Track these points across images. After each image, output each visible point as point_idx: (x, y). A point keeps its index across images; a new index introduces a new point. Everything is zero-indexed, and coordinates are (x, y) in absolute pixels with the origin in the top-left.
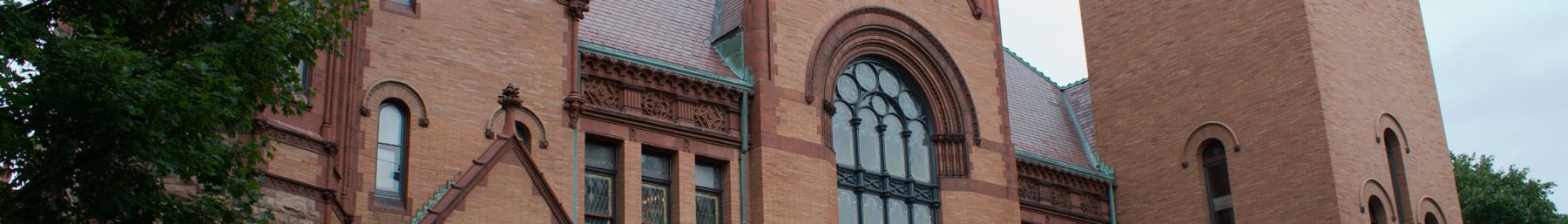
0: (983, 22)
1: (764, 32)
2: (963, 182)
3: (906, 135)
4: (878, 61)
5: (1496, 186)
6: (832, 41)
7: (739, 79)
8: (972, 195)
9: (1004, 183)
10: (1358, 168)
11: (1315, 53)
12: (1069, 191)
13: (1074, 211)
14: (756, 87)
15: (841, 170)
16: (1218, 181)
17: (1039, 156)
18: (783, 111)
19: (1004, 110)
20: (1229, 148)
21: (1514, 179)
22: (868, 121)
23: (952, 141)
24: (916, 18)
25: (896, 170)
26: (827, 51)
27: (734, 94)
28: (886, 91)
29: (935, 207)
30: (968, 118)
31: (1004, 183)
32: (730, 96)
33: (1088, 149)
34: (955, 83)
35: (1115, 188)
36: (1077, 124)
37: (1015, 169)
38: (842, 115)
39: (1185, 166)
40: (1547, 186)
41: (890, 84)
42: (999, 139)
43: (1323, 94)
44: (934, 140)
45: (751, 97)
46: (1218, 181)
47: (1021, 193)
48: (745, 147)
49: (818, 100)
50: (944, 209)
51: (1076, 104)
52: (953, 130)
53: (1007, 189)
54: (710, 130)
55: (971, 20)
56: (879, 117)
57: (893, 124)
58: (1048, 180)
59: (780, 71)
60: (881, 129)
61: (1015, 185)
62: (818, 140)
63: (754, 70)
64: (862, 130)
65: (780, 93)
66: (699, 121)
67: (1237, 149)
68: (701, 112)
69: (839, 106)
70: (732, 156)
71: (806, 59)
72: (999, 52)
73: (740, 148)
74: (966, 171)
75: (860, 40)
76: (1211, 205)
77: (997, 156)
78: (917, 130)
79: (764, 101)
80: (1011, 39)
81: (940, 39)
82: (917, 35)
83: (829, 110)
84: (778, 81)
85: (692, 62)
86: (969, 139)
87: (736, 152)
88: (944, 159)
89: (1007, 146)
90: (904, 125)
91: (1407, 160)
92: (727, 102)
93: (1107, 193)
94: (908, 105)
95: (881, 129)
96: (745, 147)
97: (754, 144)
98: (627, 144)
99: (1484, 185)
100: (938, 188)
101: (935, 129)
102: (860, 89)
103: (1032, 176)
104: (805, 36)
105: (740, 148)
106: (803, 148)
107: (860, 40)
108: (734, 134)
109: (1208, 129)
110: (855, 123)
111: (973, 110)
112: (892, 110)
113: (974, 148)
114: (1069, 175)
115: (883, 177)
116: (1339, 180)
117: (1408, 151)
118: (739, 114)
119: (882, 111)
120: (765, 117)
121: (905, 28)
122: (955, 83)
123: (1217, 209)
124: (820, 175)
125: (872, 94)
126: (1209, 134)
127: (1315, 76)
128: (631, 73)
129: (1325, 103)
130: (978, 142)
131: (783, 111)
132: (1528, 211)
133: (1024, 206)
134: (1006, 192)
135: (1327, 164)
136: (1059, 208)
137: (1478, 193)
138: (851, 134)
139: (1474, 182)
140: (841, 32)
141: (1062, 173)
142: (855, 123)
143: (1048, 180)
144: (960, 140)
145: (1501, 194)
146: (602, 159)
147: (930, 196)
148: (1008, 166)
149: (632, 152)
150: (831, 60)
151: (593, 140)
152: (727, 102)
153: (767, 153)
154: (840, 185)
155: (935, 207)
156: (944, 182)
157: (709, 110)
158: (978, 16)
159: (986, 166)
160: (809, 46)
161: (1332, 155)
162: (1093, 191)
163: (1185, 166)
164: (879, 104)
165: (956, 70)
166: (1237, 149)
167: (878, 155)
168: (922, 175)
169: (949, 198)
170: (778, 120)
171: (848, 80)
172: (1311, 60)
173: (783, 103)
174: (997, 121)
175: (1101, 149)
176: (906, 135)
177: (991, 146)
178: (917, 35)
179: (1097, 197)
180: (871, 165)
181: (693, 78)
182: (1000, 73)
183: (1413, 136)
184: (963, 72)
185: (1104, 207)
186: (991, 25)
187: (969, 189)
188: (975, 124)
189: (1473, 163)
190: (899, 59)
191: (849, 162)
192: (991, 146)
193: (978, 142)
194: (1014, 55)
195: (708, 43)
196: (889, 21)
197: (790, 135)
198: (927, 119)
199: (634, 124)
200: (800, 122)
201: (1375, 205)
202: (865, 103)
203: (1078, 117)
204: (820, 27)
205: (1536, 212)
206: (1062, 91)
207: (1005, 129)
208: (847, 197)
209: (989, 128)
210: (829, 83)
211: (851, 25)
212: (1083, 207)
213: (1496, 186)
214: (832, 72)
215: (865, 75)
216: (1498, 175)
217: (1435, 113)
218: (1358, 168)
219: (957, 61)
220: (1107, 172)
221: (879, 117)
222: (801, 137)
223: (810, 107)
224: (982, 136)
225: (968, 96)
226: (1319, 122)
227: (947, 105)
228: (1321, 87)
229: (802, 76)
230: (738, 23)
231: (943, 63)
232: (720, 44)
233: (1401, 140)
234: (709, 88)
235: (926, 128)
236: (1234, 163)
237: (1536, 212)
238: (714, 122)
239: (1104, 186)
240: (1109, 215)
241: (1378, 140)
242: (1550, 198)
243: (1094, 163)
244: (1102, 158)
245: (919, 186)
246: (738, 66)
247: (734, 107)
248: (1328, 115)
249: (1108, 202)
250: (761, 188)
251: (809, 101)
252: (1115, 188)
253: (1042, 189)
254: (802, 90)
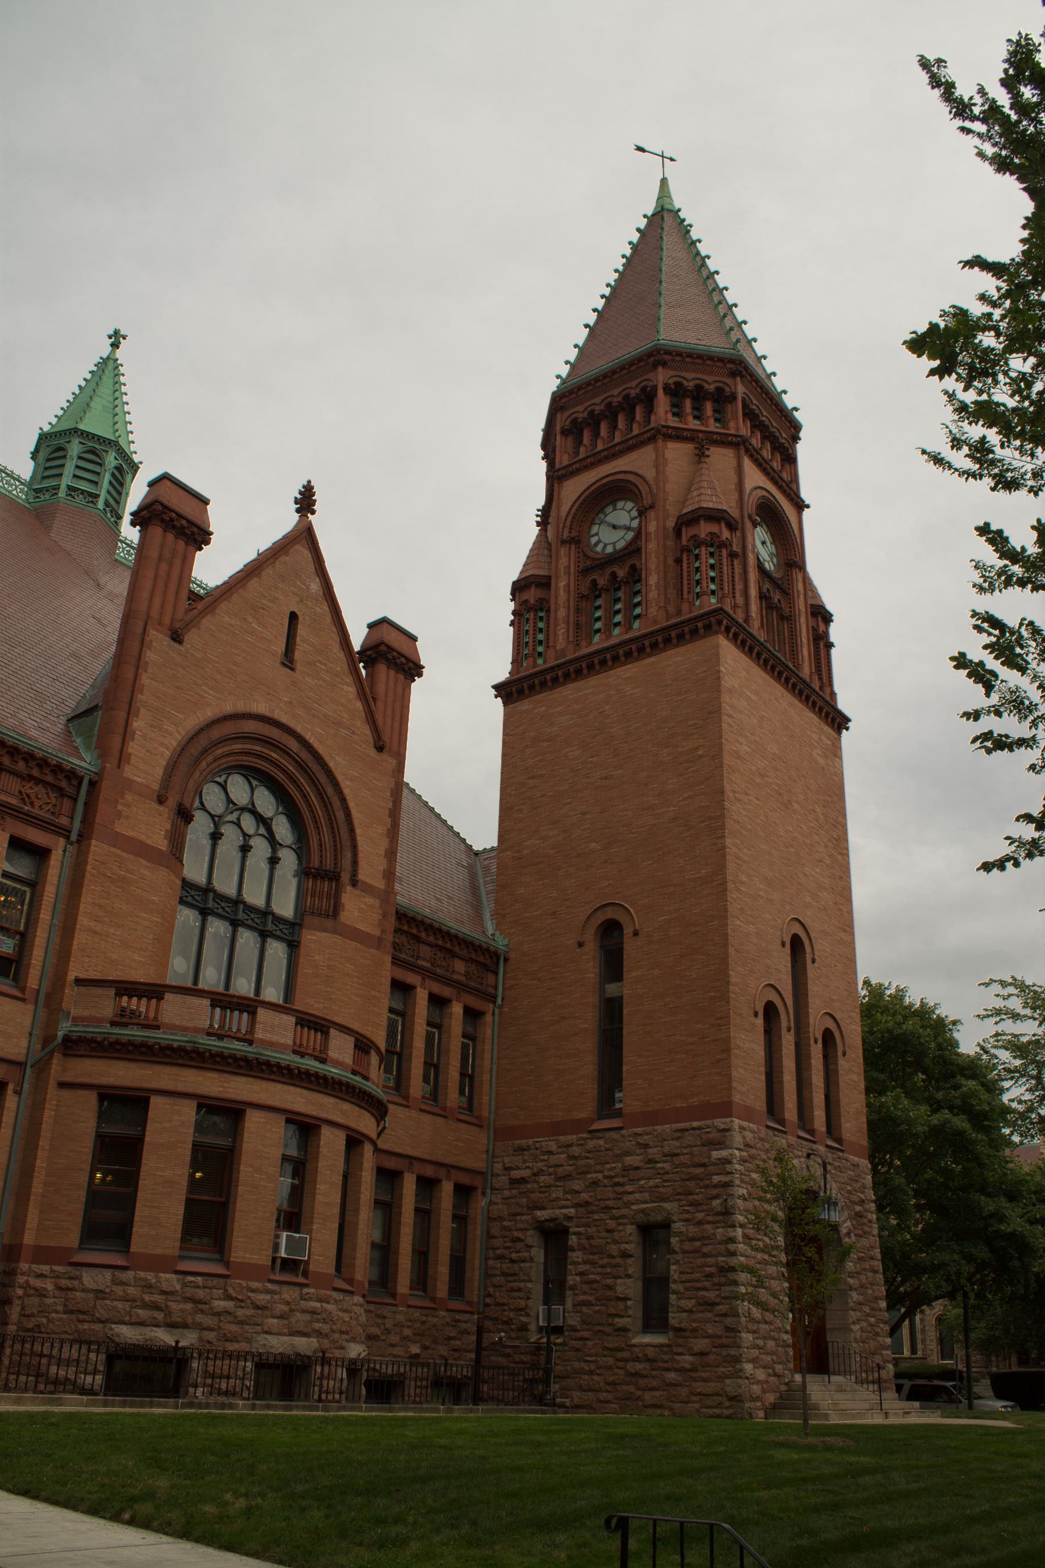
0: (384, 756)
1: (123, 715)
2: (329, 923)
3: (274, 861)
4: (255, 774)
5: (905, 1017)
6: (203, 741)
7: (85, 761)
8: (338, 939)
9: (376, 932)
10: (757, 970)
11: (728, 841)
12: (454, 955)
13: (455, 977)
14: (100, 774)
15: (186, 884)
16: (613, 965)
17: (427, 912)
18: (128, 806)
19: (391, 855)
20: (628, 931)
21: (924, 1013)
22: (231, 836)
23: (325, 877)
24: (312, 740)
25: (255, 896)
26: (195, 750)
27: (73, 776)
28: (259, 809)
29: (293, 946)
30: (348, 855)
31: (376, 932)
32: (68, 778)
33: (487, 915)
34: (340, 815)
35: (506, 960)
36: (483, 890)
37: (393, 919)
38: (200, 827)
39: (580, 945)
40: (954, 1023)
41: (266, 802)
42: (380, 884)
43: (730, 885)
44: (305, 872)
45: (92, 784)
46: (613, 965)
47: (396, 946)
48: (74, 837)
49: (172, 801)
50: (303, 950)
51: (486, 869)
52: (329, 864)
53: (380, 939)
54: (36, 811)
55: (373, 753)
56: (245, 834)
57: (260, 848)
58: (431, 939)
59: (133, 760)
60: (245, 849)
61: (390, 937)
62: (163, 845)
63: (103, 752)
64: (222, 846)
65: (129, 784)
66: (24, 798)
67: (636, 934)
68: (29, 788)
69: (199, 817)
70: (58, 847)
71: (168, 754)
72: (399, 787)
73: (68, 838)
74: (335, 911)
75: (238, 747)
76: (602, 990)
77: (376, 902)
78: (289, 860)
79: (105, 791)
80: (410, 776)
81: (331, 765)
82: (305, 755)
83: (184, 816)
84: (128, 772)
85: (34, 733)
86: (345, 877)
87: (62, 841)
88: (313, 895)
89: (387, 895)
90: (274, 850)
91: (811, 971)
92: (64, 784)
93: (497, 964)
94: (283, 829)
95: (245, 849)
96: (74, 837)
97: (84, 837)
98: (419, 989)
99: (894, 1015)
100: (301, 925)
101: (309, 861)
102: (229, 801)
103: (411, 928)
104: (172, 728)
105: (68, 838)
106: (142, 850)
107: (238, 747)
108: (64, 821)
109: (609, 909)
110: (216, 837)
111: (354, 847)
112: (262, 830)
113: (349, 888)
114: (456, 937)
115: (237, 902)
116: (734, 978)
117: (813, 961)
118: (75, 800)
119: (251, 831)
120: (103, 808)
121: (293, 745)
122: (340, 815)
123: (607, 995)
124: (157, 884)
125: (243, 809)
126: (610, 914)
127: (724, 866)
128: (40, 766)
129: (732, 895)
130: (354, 883)
131: (128, 806)
132: (933, 1045)
133: (396, 961)
134: (379, 943)
135: (724, 959)
136: (438, 971)
137: (886, 1021)
138: (267, 872)
139: (886, 1010)
140: (216, 733)
141: (448, 933)
142: (216, 837)
143: (431, 939)
144: (334, 877)
145: (909, 1025)
146: (22, 868)
147: (291, 934)
148: (385, 915)
149: (422, 997)
150: (198, 761)
151: (17, 844)
152: (64, 784)
153: (97, 848)
154: (182, 901)
155: (293, 946)
156: (308, 920)
157: (40, 789)
158: (380, 749)
159: (358, 909)
160: (174, 739)
161: (732, 951)
162: (481, 959)
163: (580, 945)
164: (248, 823)
165: (343, 800)
166: (636, 934)
167: (236, 878)
168: (285, 907)
169: (312, 938)
170: (119, 815)
171: (216, 789)
172: (724, 848)
173: (129, 797)
174: (381, 865)
175: (499, 916)
176: (274, 861)
177: (369, 890)
178: (305, 755)
179: (484, 966)
180: (226, 886)
181: (25, 748)
182: (395, 814)
183: (821, 946)
184: (351, 805)
185: (490, 979)
186: (394, 762)
187: (335, 932)
188: (355, 863)
189: (888, 992)
190: (280, 777)
191: (201, 879)
192: (369, 890)
193: (354, 883)
194: (413, 791)
195: (63, 720)
196: (275, 733)
197: (131, 834)
198: (302, 847)
199: (427, 974)
200: (152, 826)
201: (770, 1011)
202: (233, 817)
203: (486, 883)
204: (193, 722)
205: (940, 1048)
206: (477, 854)
207: (389, 875)
208: (188, 917)
209: (371, 870)
210: (191, 785)
211: (229, 728)
212: (467, 974)
213: (905, 1017)
214: (197, 774)
215: (239, 789)
216: (911, 1005)
217: (847, 926)
218: (757, 970)
219: (346, 791)
220: (501, 942)
221: (245, 834)
222: (142, 837)
223: (161, 808)
224: (361, 876)
225: (352, 831)
226: (722, 914)
227: (327, 838)
228: (729, 878)
229: (159, 772)
230: (99, 701)
231: (330, 790)
232: (76, 722)
233: (808, 949)
234: (43, 763)
235: (299, 858)
236: (630, 947)
237: (940, 1048)
238: (43, 802)
239: (494, 955)
240: (496, 988)
241: (783, 944)
242: (956, 1035)
243: (490, 931)
244: (498, 926)
245: (278, 920)
246: (88, 748)
247: (70, 790)
248: (733, 908)
249: (496, 974)
250: (81, 885)
251: (161, 800)
252: (506, 960)
253: (423, 947)
254: (156, 787)
